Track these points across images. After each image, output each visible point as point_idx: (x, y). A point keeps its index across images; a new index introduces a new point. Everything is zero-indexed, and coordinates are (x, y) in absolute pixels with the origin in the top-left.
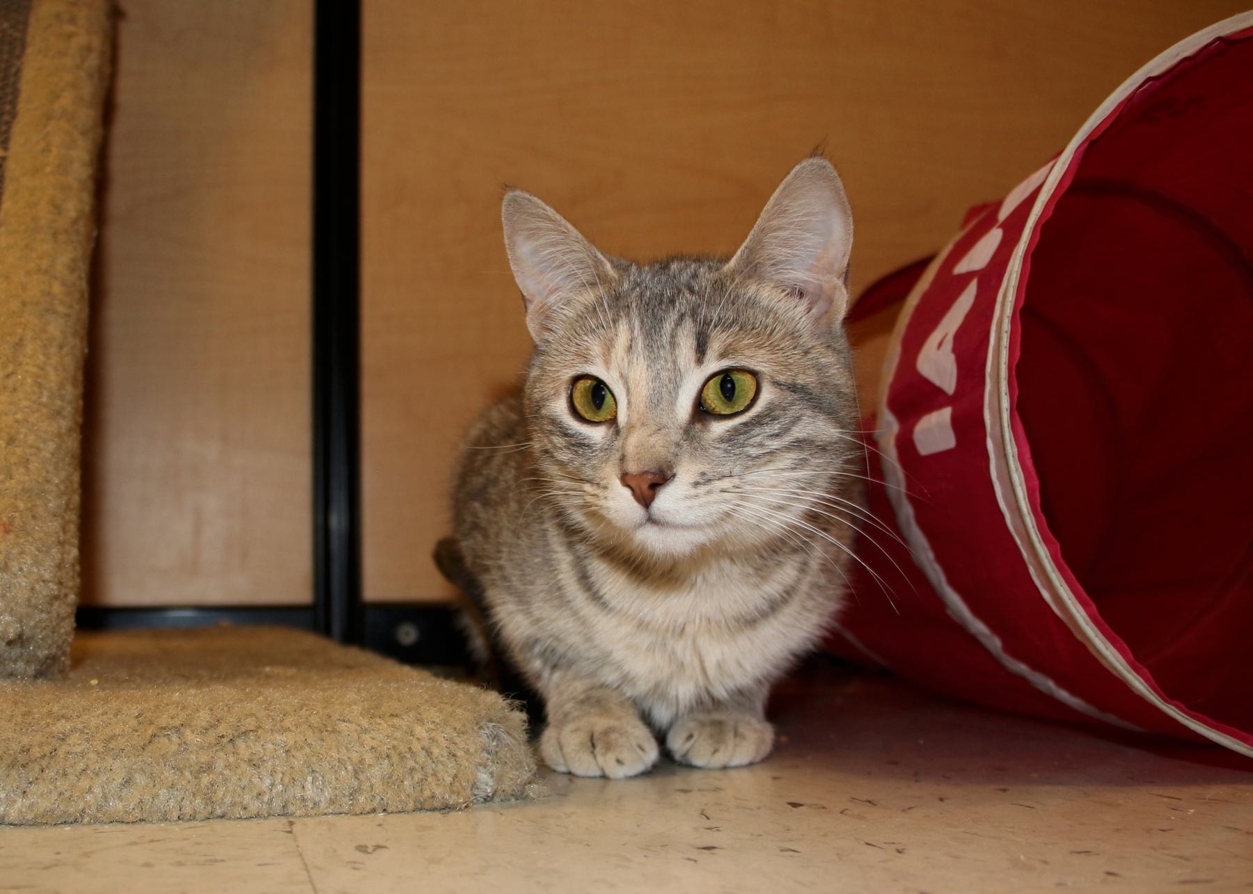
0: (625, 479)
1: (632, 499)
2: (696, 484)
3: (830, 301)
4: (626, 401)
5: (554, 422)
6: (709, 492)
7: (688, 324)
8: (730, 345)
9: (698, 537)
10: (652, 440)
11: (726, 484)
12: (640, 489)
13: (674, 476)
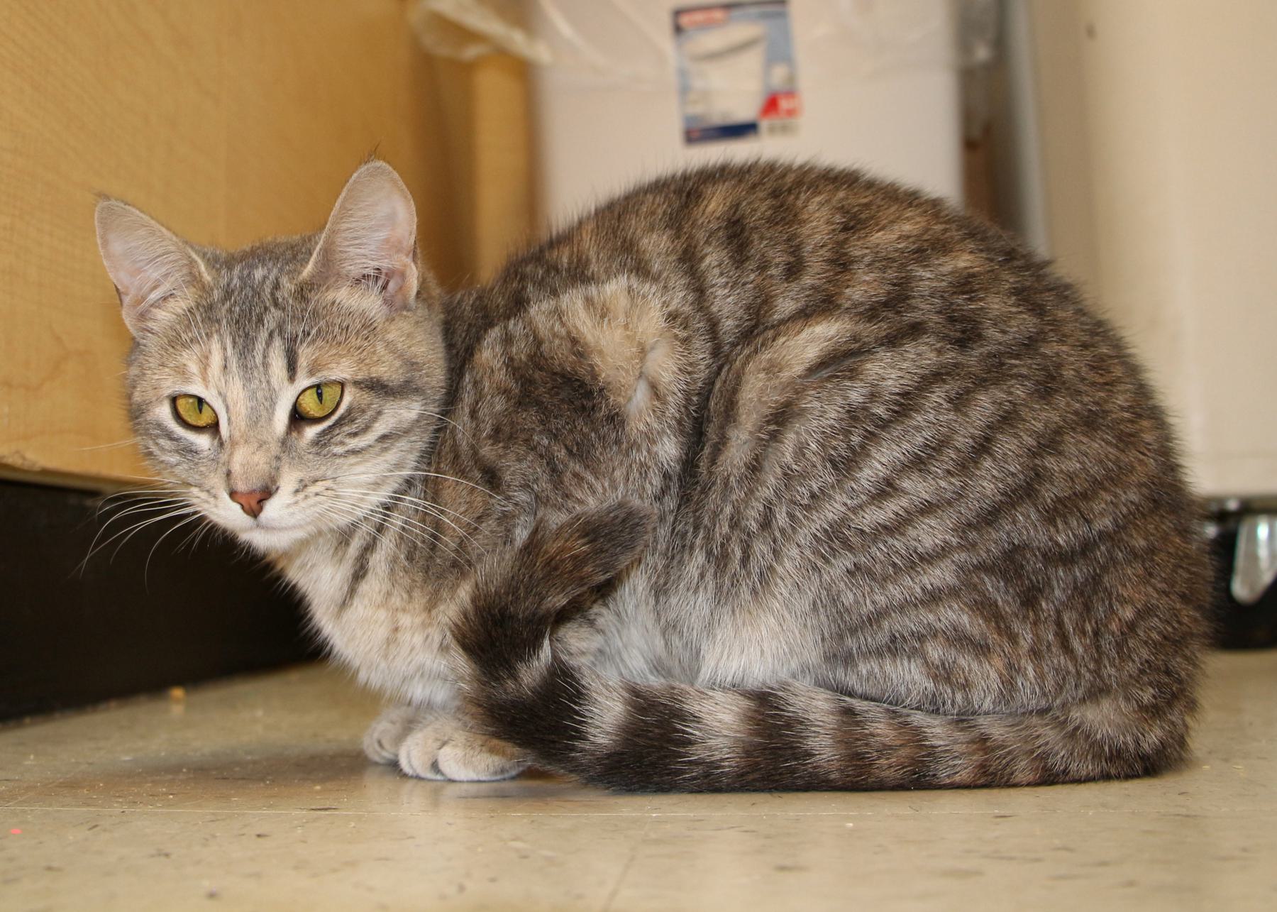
0: (233, 494)
1: (241, 511)
2: (297, 491)
3: (403, 275)
4: (226, 417)
5: (159, 425)
6: (306, 497)
7: (277, 342)
8: (317, 359)
9: (300, 534)
10: (256, 458)
11: (319, 487)
12: (250, 505)
13: (277, 489)
